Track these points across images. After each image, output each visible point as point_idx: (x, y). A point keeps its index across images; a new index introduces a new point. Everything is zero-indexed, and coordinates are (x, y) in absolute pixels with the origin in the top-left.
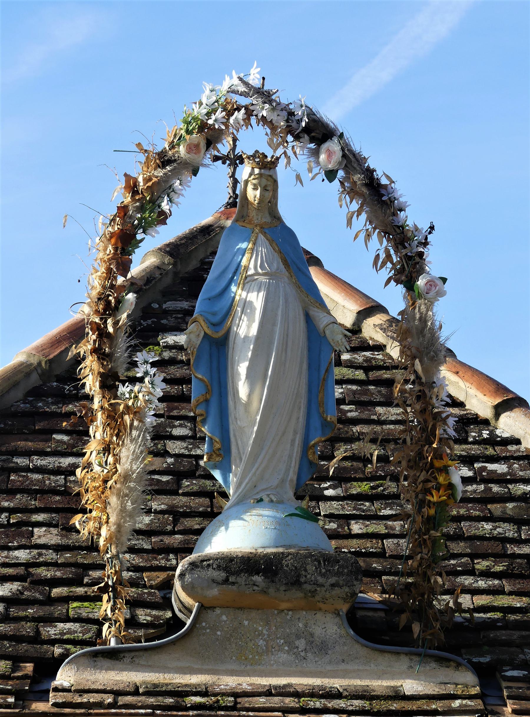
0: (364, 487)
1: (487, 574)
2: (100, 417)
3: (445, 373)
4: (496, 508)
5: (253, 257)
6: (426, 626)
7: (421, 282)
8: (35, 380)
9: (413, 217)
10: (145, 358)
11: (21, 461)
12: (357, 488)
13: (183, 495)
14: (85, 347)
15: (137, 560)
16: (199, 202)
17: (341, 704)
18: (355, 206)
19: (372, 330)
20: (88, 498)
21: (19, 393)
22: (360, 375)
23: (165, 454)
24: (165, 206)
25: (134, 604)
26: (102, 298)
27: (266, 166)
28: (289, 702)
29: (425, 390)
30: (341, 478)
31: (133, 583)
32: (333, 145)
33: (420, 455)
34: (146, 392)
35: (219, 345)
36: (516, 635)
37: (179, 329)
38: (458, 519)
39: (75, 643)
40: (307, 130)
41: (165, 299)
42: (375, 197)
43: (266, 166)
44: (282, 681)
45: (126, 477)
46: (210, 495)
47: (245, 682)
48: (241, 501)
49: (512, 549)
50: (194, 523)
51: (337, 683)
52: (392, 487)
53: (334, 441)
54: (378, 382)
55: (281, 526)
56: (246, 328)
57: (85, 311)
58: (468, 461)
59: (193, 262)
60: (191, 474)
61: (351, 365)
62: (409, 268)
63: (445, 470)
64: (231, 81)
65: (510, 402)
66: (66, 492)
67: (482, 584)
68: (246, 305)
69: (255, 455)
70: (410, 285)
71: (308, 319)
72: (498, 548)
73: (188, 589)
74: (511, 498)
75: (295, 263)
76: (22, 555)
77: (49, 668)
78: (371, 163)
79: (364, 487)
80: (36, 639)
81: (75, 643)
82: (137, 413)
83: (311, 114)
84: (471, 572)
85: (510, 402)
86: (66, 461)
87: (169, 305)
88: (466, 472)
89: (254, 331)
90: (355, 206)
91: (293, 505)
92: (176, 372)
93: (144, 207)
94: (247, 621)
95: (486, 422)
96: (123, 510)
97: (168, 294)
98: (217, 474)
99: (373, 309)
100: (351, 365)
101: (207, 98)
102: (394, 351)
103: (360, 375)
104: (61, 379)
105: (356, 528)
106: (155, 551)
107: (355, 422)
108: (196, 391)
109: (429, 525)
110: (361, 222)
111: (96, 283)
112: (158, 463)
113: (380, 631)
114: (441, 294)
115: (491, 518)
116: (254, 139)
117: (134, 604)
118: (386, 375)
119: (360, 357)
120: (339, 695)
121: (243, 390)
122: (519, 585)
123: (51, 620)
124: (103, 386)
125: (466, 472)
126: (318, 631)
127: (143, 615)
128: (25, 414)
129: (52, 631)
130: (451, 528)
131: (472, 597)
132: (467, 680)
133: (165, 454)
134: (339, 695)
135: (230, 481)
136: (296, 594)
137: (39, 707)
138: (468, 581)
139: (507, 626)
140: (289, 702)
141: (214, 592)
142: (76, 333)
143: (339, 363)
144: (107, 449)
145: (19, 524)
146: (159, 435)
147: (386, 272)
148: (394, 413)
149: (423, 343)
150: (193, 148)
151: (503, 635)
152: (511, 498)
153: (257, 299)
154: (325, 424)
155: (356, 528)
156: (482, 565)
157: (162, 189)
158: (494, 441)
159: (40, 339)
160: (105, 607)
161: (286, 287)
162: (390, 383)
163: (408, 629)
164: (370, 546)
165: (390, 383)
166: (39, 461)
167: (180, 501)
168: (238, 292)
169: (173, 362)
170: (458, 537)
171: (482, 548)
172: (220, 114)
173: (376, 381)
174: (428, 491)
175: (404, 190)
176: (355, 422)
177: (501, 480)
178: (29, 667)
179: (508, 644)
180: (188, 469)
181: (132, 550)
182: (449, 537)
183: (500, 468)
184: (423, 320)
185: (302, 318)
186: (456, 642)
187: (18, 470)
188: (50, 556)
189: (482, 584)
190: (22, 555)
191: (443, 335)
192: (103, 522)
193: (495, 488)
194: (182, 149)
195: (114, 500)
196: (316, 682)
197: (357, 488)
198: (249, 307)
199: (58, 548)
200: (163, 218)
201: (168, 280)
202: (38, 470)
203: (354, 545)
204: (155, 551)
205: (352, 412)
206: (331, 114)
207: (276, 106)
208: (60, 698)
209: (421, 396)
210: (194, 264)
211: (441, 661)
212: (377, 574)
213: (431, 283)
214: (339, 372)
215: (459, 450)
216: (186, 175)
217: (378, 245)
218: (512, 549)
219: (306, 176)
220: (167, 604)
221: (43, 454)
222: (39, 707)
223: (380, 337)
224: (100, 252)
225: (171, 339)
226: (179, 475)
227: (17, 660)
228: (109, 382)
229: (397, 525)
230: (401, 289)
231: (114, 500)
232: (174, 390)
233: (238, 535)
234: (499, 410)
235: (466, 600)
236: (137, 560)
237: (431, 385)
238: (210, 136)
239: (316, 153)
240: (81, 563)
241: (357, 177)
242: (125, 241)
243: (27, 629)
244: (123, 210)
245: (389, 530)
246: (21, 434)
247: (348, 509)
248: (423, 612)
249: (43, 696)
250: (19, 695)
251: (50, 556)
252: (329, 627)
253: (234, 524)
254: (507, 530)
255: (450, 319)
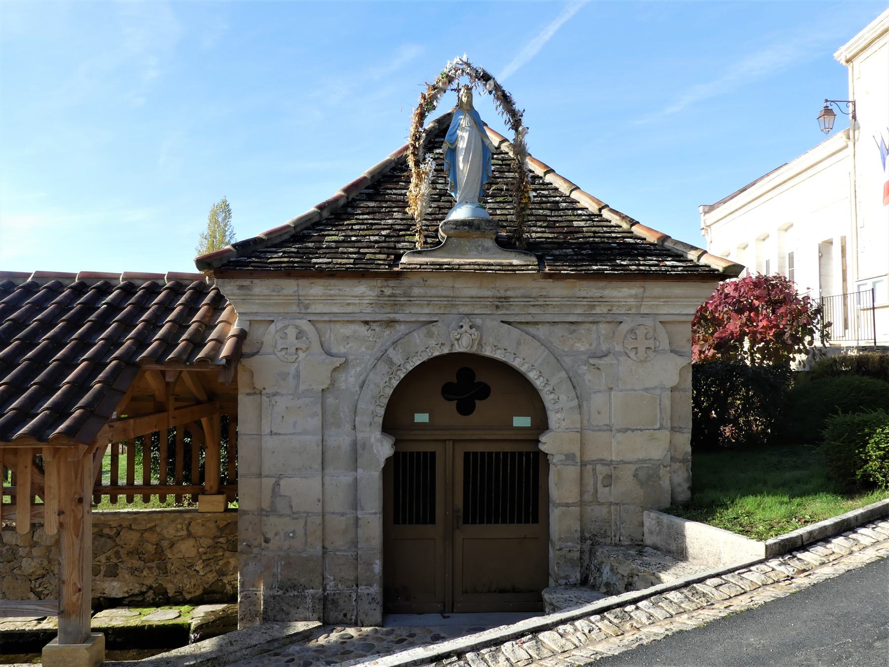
0: (501, 199)
1: (540, 227)
2: (414, 175)
3: (528, 160)
4: (544, 206)
5: (464, 121)
6: (521, 242)
7: (520, 129)
8: (393, 165)
9: (518, 107)
10: (429, 157)
11: (389, 191)
12: (499, 199)
13: (441, 201)
14: (409, 152)
15: (427, 223)
16: (446, 104)
17: (493, 267)
18: (498, 103)
19: (504, 147)
20: (411, 202)
21: (388, 169)
22: (500, 162)
23: (436, 189)
24: (435, 103)
25: (426, 237)
26: (414, 135)
27: (469, 89)
28: (476, 267)
29: (521, 165)
30: (493, 196)
31: (426, 230)
32: (491, 82)
33: (519, 187)
34: (429, 166)
35: (453, 151)
36: (549, 246)
37: (440, 148)
38: (532, 209)
39: (407, 249)
40: (482, 77)
41: (436, 138)
42: (505, 100)
43: (469, 89)
44: (474, 261)
45: (423, 195)
46: (451, 202)
47: (462, 261)
48: (460, 203)
49: (549, 218)
50: (445, 211)
51: (492, 261)
52: (510, 199)
53: (491, 184)
54: (506, 165)
55: (473, 210)
56: (462, 145)
57: (409, 141)
58: (535, 190)
59: (444, 125)
60: (444, 195)
61: (497, 159)
62: (516, 124)
63: (527, 192)
64: (457, 60)
65: (550, 171)
66: (404, 201)
67: (539, 230)
68: (462, 137)
69: (465, 188)
70: (517, 130)
71: (483, 142)
72: (544, 218)
73: (443, 231)
74: (549, 202)
75: (479, 125)
76: (390, 221)
77: (399, 257)
78: (504, 88)
79: (501, 199)
80: (395, 248)
81: (407, 249)
82: (426, 174)
83: (484, 71)
84: (535, 226)
85: (550, 171)
86: (404, 191)
87: (437, 140)
88: (535, 194)
89: (465, 146)
90: (498, 103)
91: (478, 204)
92: (440, 162)
93: (428, 104)
94: (462, 241)
95: (541, 178)
96: (422, 205)
97: (437, 136)
98: (453, 194)
99: (505, 140)
100: (497, 159)
101: (449, 66)
102: (511, 154)
103: (500, 162)
104: (402, 165)
105: (498, 212)
106: (433, 220)
107: (498, 178)
108: (445, 168)
109: (522, 210)
110: (501, 108)
111: (412, 130)
112: (434, 192)
113: (505, 245)
114: (527, 133)
115: (542, 209)
116: (465, 80)
117: (426, 237)
118: (509, 162)
119: (500, 156)
120: (492, 265)
121: (461, 165)
122: (551, 230)
123: (399, 242)
124: (415, 165)
125: (535, 194)
126: (486, 245)
127: (429, 240)
128: (390, 176)
129: (399, 246)
130: (529, 212)
131: (536, 234)
132: (534, 260)
133: (436, 189)
134: (492, 265)
135: (457, 196)
136: (478, 232)
137: (396, 269)
138: (534, 229)
139: (547, 243)
140: (476, 267)
141: (452, 232)
142: (407, 148)
143: (493, 158)
144: (417, 186)
145: (389, 212)
146: (434, 183)
147: (509, 126)
148: (511, 175)
149: (520, 149)
150: (444, 83)
151: (545, 246)
152: (549, 202)
153: (466, 135)
154: (488, 177)
155: (498, 212)
156: (539, 224)
157: (434, 97)
158: (543, 184)
159: (394, 152)
160: (417, 237)
161: (475, 130)
162: (509, 165)
163: (515, 244)
164: (503, 218)
165: (509, 165)
166: (395, 191)
167: (441, 204)
168: (459, 133)
169: (438, 158)
170: (532, 215)
171: (539, 218)
172: (453, 71)
173: (505, 164)
174: (521, 199)
175: (515, 98)
176: (498, 178)
177: (546, 196)
178: (393, 257)
179: (547, 249)
180: (443, 194)
181: (425, 220)
182: (529, 215)
183: (546, 192)
184: (521, 142)
185: (319, 343)
186: (530, 248)
187: (388, 194)
188: (399, 222)
189: (539, 230)
190: (390, 221)
191: (527, 147)
192: (415, 209)
193: (544, 199)
194: (440, 84)
195: (419, 203)
196: (485, 261)
197: (499, 199)
198: (463, 138)
199: (401, 219)
200: (434, 108)
201: (437, 131)
202: (394, 194)
203: (497, 218)
204: (433, 220)
205: (497, 174)
206: (490, 72)
207: (472, 69)
208: (403, 266)
209: (520, 168)
210: (445, 126)
211: (525, 254)
212: (505, 227)
213: (523, 129)
214: (493, 161)
215: (533, 187)
216: (442, 93)
217: (506, 116)
218: (549, 218)
219: (482, 93)
220: (437, 237)
221: (396, 189)
222: (396, 269)
223: (507, 150)
224: (414, 119)
225: (438, 151)
226: (440, 195)
227: (389, 255)
228: (417, 164)
229: (512, 211)
230: (514, 131)
231: (419, 203)
232: (439, 168)
233: (461, 213)
234: (546, 173)
235: (534, 235)
236: (427, 223)
237: (523, 164)
238: (450, 79)
239: (485, 85)
240: (409, 223)
241: (499, 93)
242: (422, 116)
243: (392, 245)
244: (421, 105)
245: (508, 212)
246: (389, 183)
247: (496, 206)
248: (520, 238)
249: (397, 266)
250: (389, 265)
251: (399, 222)
252: (489, 243)
253: (458, 210)
254: (548, 212)
255: (531, 142)
